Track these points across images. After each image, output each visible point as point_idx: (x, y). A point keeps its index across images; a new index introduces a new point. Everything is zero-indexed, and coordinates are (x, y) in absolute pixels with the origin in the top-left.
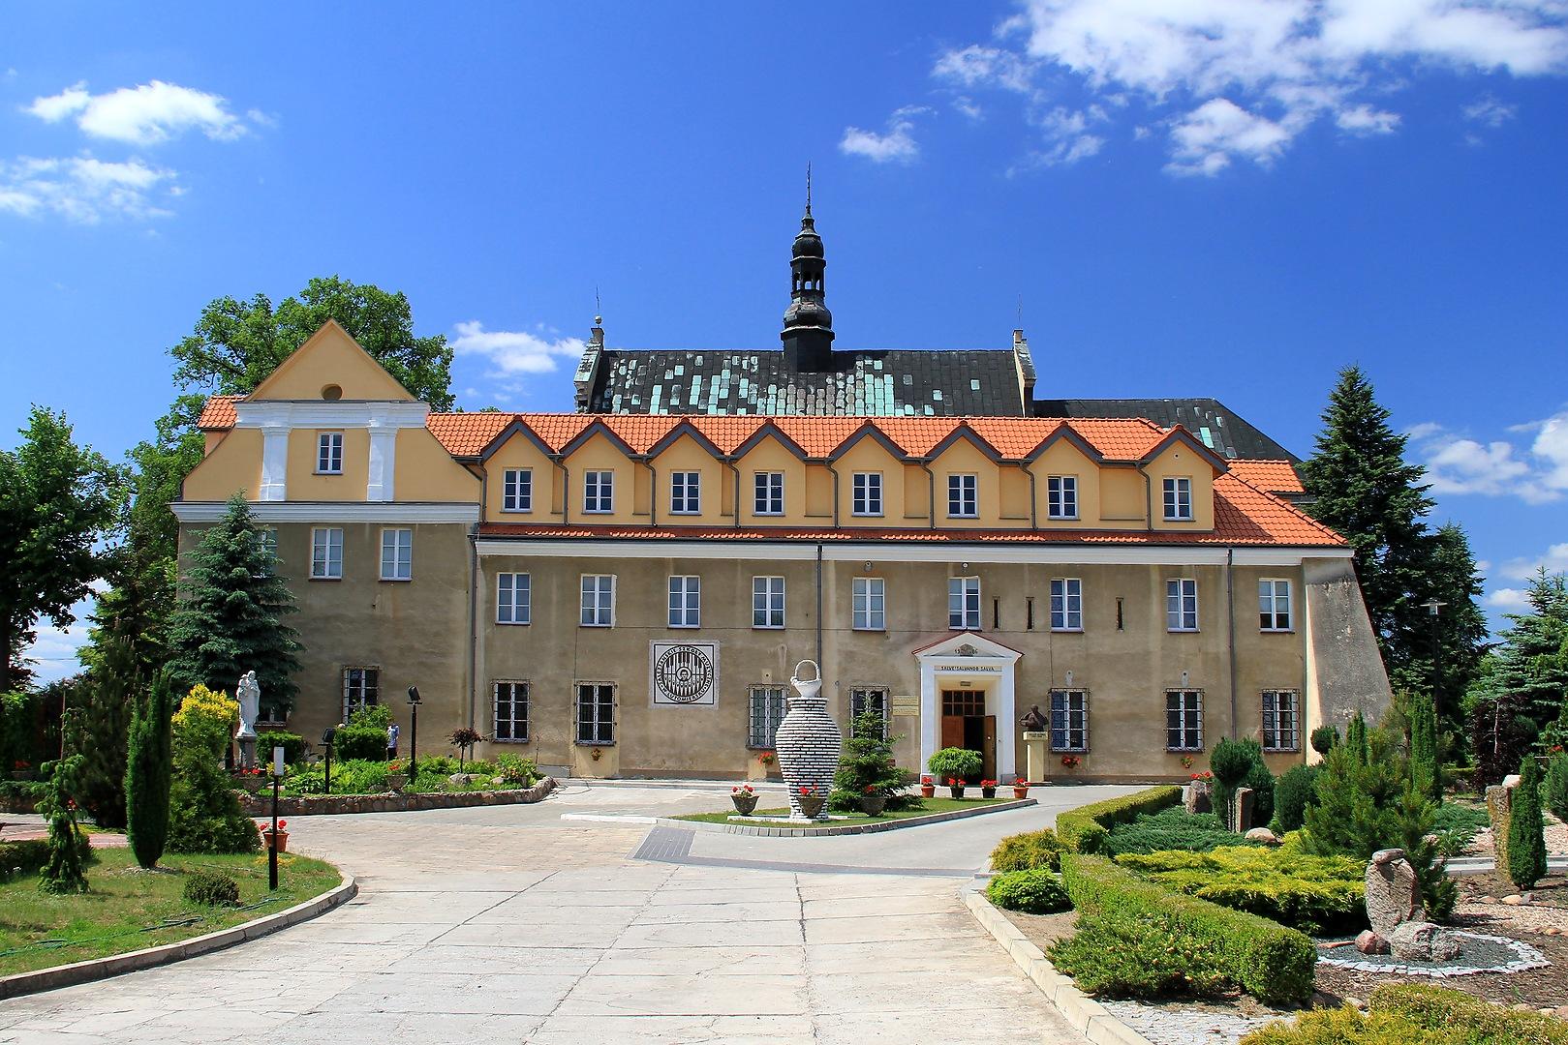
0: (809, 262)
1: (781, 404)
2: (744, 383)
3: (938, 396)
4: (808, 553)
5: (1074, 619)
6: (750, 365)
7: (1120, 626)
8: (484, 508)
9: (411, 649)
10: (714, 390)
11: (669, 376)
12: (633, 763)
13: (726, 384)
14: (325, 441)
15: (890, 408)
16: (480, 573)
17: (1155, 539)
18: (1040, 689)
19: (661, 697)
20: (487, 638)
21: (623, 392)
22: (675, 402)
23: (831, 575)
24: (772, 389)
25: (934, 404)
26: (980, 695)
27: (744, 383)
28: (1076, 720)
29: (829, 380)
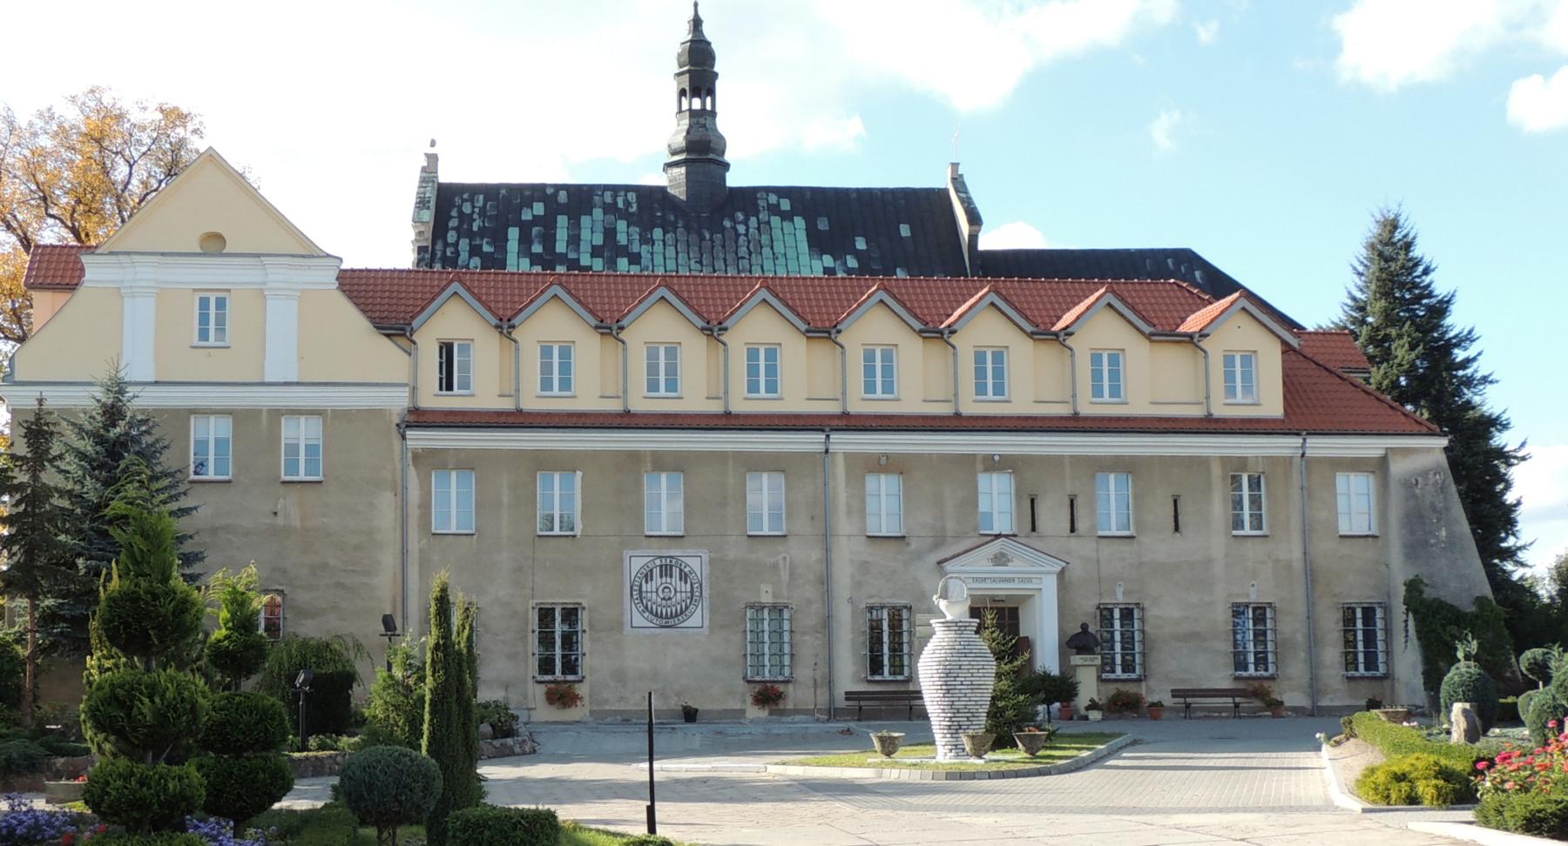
0: (699, 68)
1: (671, 252)
2: (622, 225)
3: (861, 244)
4: (810, 442)
5: (1257, 522)
6: (628, 204)
7: (1177, 529)
8: (414, 390)
9: (325, 566)
10: (585, 234)
11: (526, 216)
12: (606, 701)
13: (599, 227)
14: (204, 303)
15: (805, 259)
16: (412, 472)
17: (1211, 426)
18: (1086, 606)
19: (639, 620)
20: (421, 551)
21: (471, 235)
22: (537, 248)
23: (840, 468)
24: (658, 233)
25: (858, 254)
26: (1014, 612)
27: (622, 225)
28: (1128, 641)
29: (727, 224)
